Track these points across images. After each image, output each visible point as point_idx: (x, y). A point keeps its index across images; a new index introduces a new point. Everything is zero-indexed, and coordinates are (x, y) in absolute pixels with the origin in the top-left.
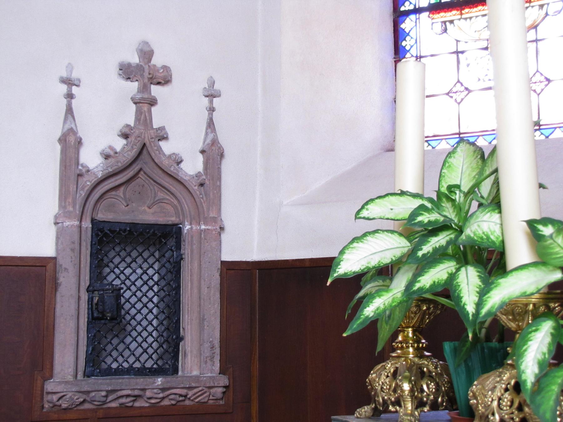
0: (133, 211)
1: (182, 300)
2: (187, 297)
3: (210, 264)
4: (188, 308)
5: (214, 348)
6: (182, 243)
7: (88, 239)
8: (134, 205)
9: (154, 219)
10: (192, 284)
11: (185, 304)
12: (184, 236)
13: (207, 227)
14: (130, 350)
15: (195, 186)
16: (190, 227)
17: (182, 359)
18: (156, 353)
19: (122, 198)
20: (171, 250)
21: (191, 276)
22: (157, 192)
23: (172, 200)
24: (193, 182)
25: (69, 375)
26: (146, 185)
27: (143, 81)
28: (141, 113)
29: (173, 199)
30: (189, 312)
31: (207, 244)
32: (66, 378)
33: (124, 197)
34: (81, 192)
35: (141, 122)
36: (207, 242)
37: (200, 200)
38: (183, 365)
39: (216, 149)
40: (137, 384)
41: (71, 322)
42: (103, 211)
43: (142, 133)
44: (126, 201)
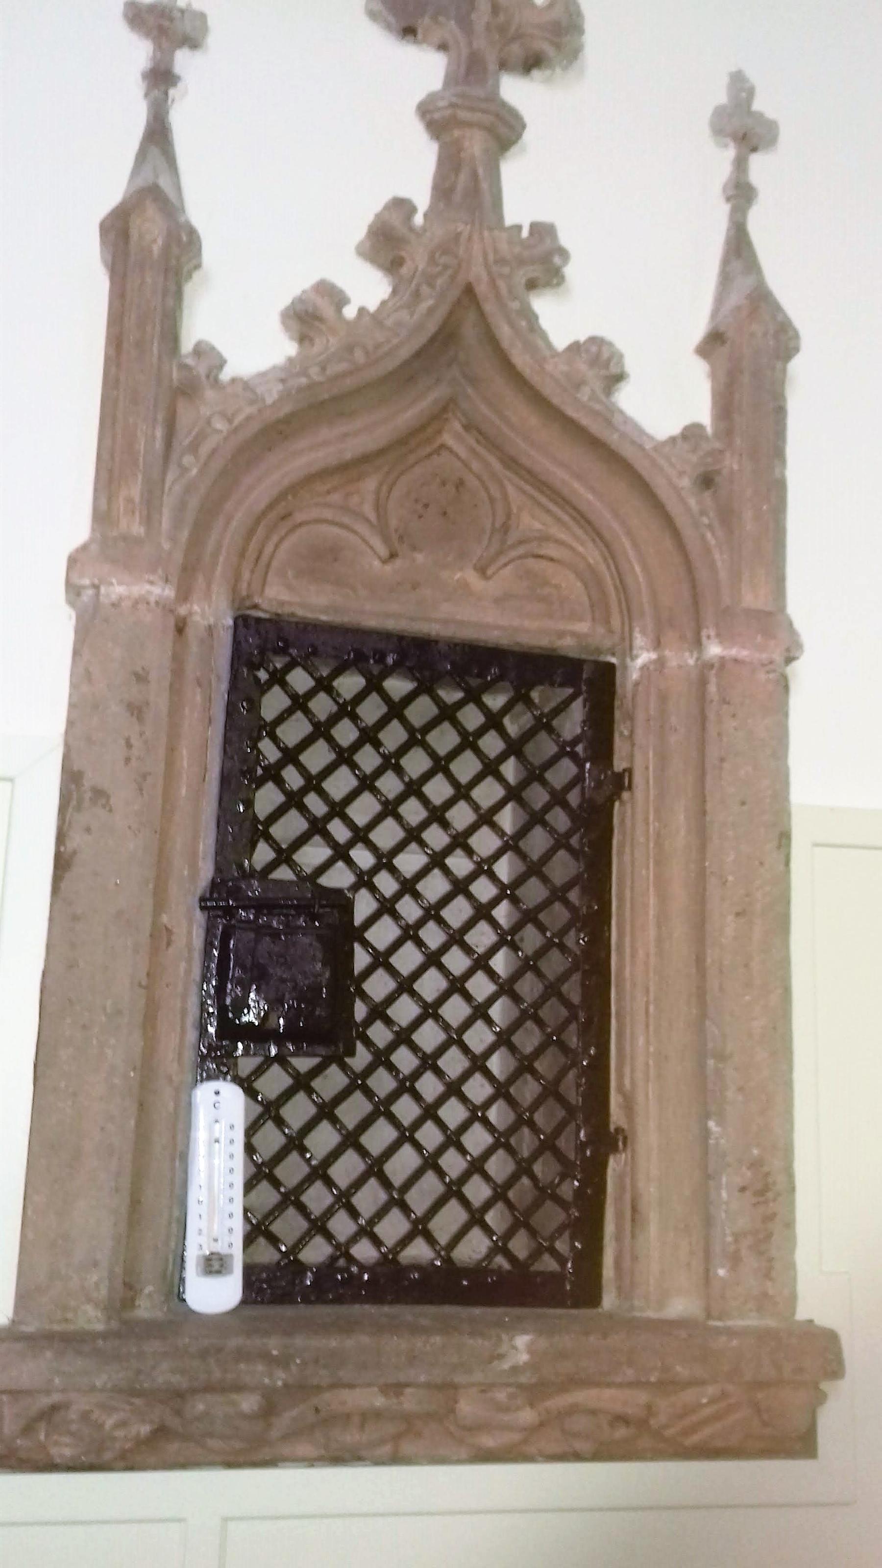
0: (415, 586)
1: (621, 968)
2: (641, 953)
3: (745, 808)
4: (647, 1003)
5: (770, 1195)
6: (621, 729)
7: (213, 677)
8: (420, 557)
9: (504, 622)
10: (663, 898)
11: (634, 985)
12: (629, 696)
13: (734, 652)
14: (386, 1183)
15: (681, 474)
16: (653, 656)
17: (619, 1238)
18: (500, 1205)
19: (367, 520)
20: (574, 756)
21: (657, 863)
22: (515, 511)
23: (580, 549)
24: (673, 460)
25: (89, 1300)
26: (472, 482)
27: (470, 44)
28: (457, 168)
29: (582, 544)
30: (652, 1021)
31: (734, 724)
32: (70, 1315)
33: (379, 516)
34: (188, 460)
35: (457, 197)
36: (734, 716)
37: (703, 538)
38: (627, 1263)
39: (765, 334)
40: (412, 1359)
41: (113, 1041)
42: (290, 574)
43: (458, 235)
44: (386, 540)
